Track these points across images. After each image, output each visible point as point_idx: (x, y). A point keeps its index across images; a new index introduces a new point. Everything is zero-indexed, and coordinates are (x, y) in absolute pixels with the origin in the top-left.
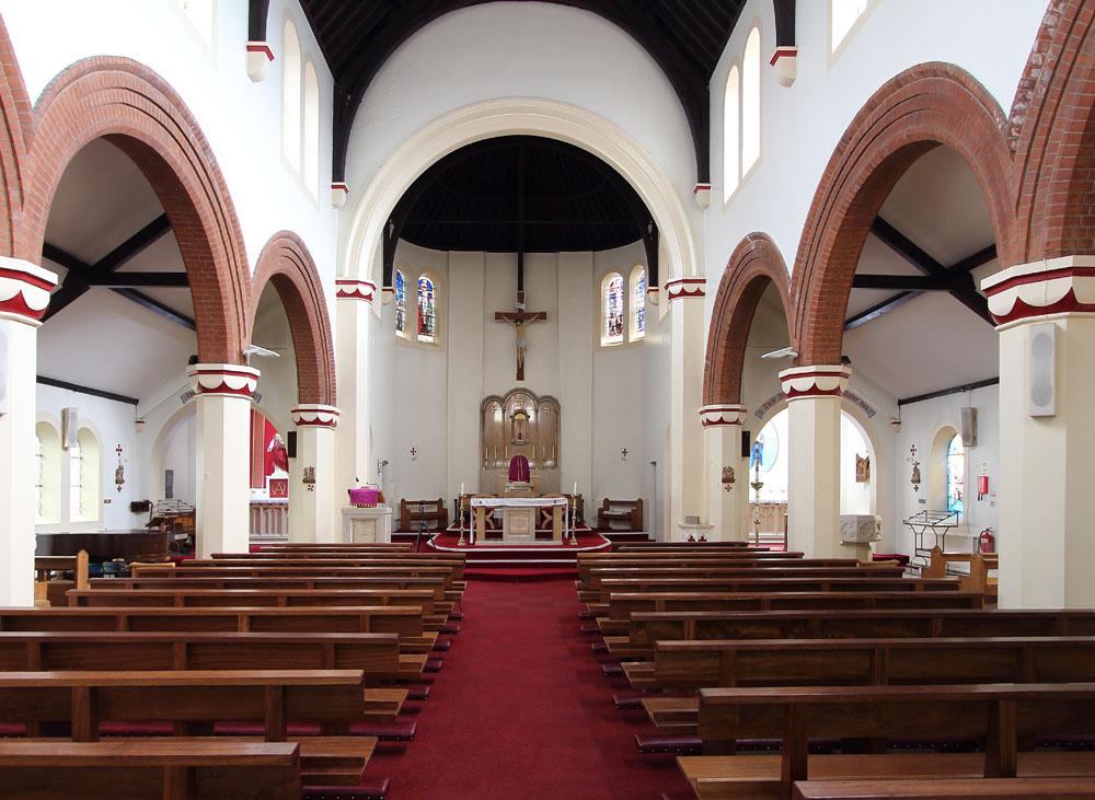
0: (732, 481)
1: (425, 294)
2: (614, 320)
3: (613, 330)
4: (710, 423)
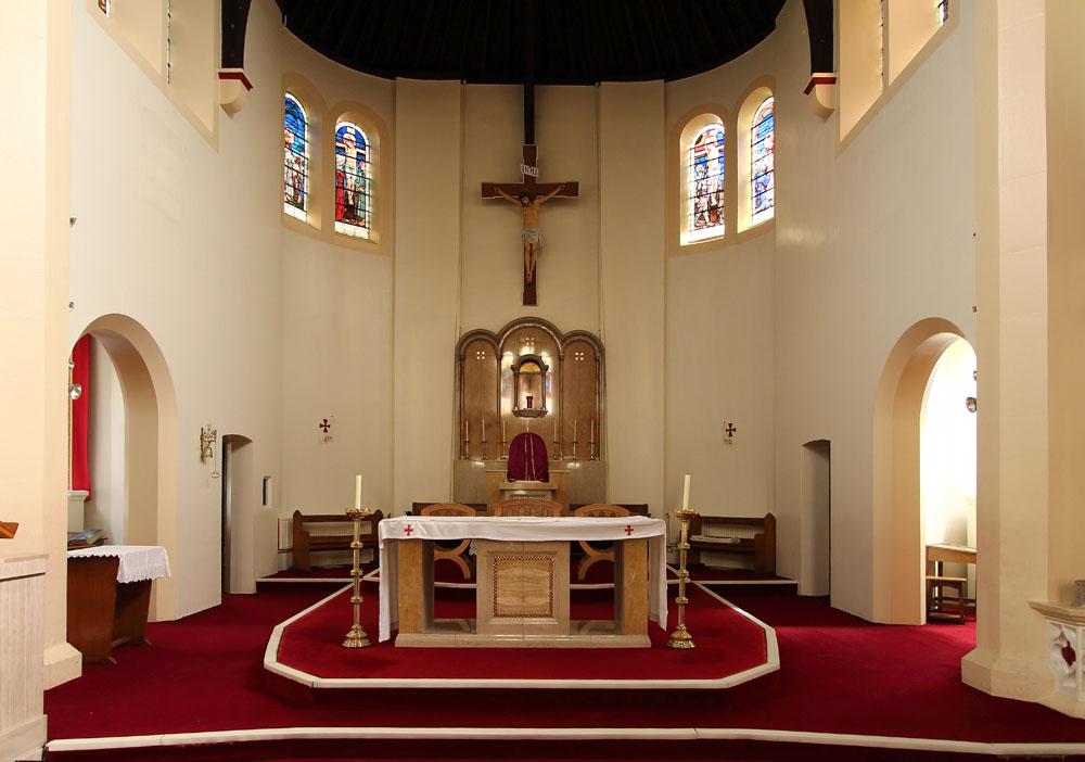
1: (353, 152)
2: (704, 200)
3: (702, 218)
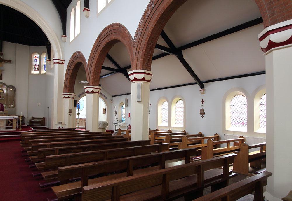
0: (72, 113)
3: (35, 69)
4: (65, 97)
